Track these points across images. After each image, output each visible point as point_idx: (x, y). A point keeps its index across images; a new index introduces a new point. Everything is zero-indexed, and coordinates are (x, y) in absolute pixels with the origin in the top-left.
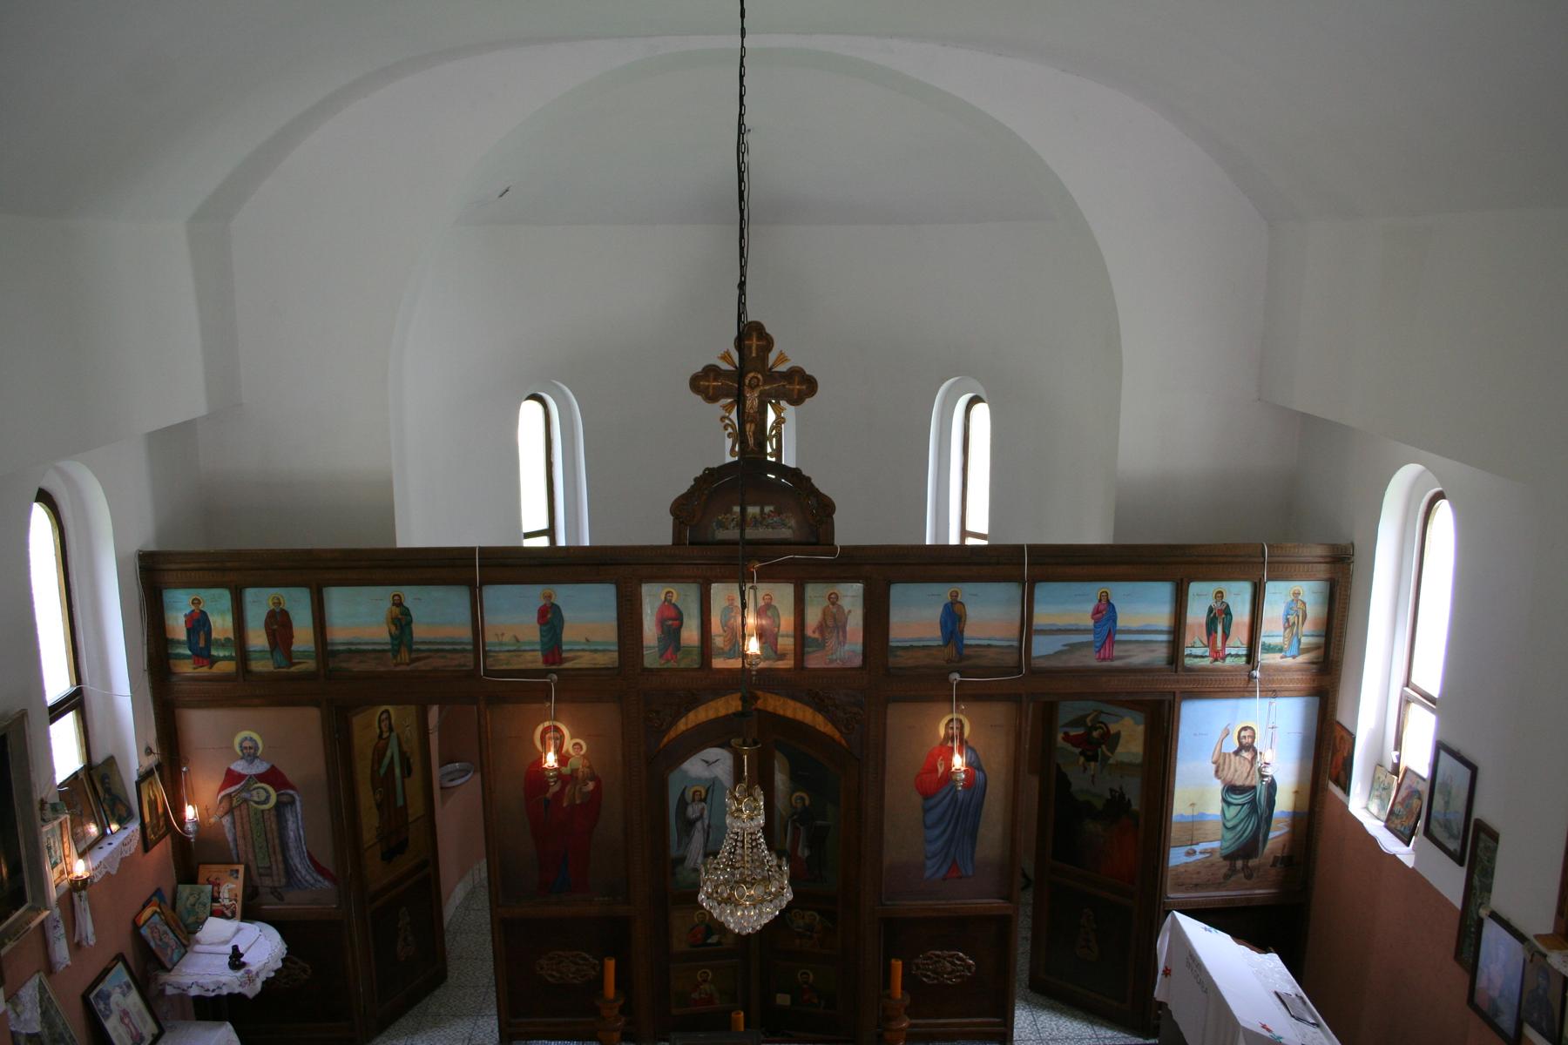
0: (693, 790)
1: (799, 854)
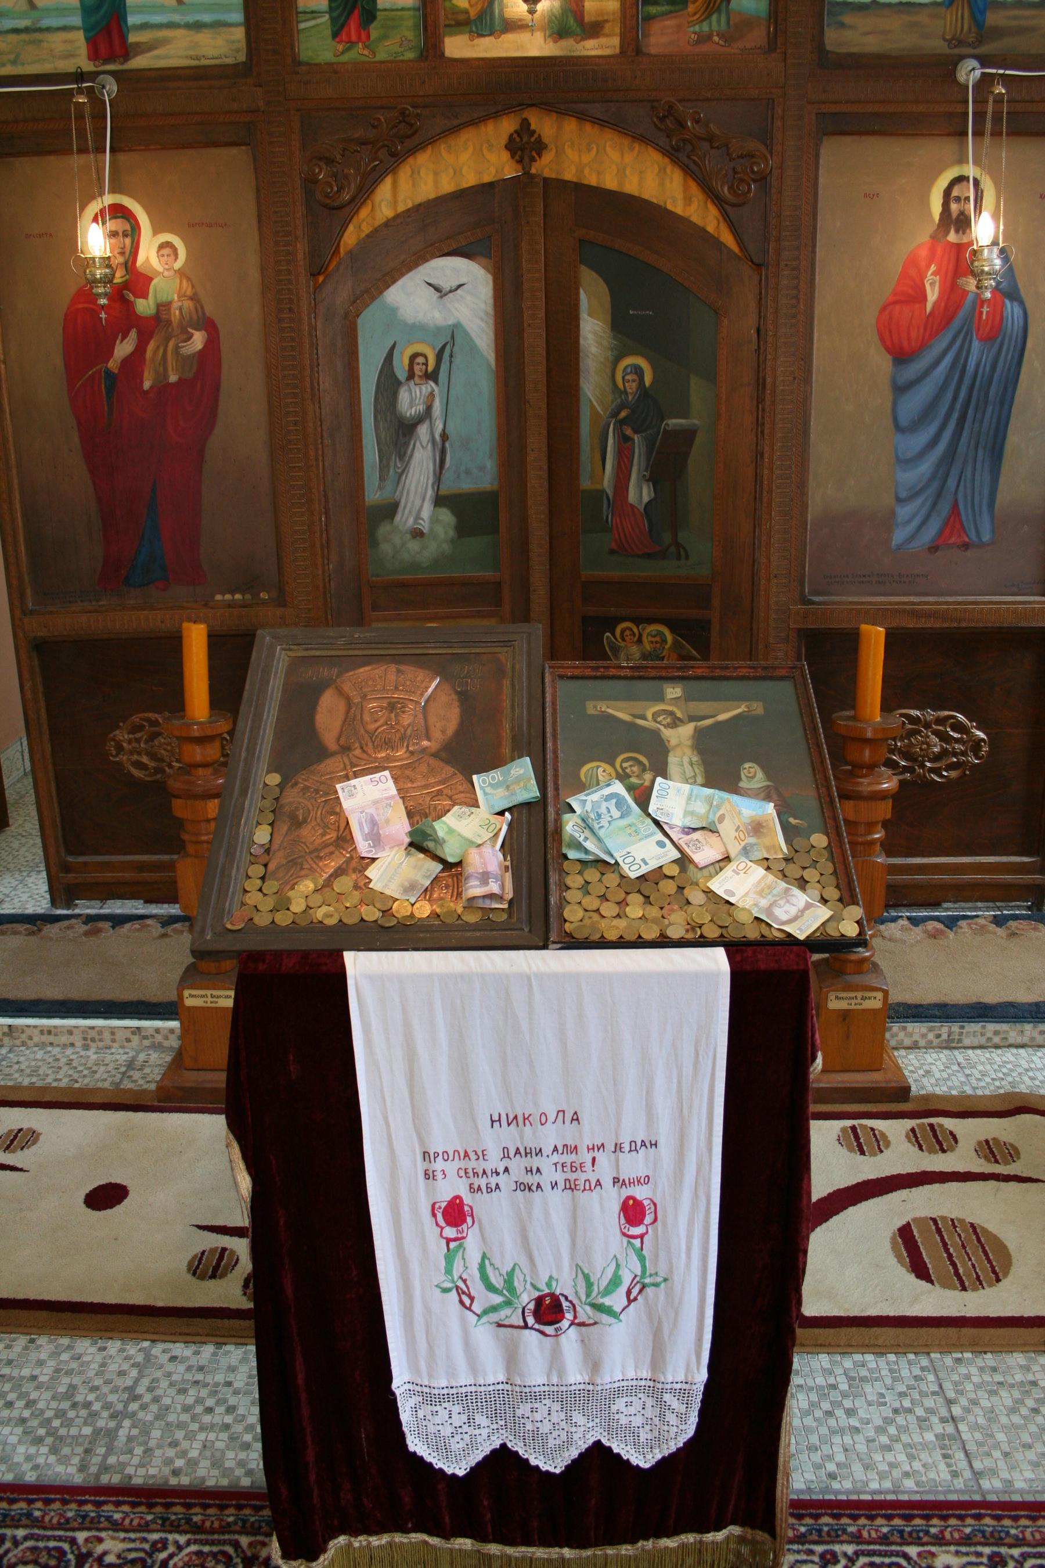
0: (409, 352)
1: (632, 497)
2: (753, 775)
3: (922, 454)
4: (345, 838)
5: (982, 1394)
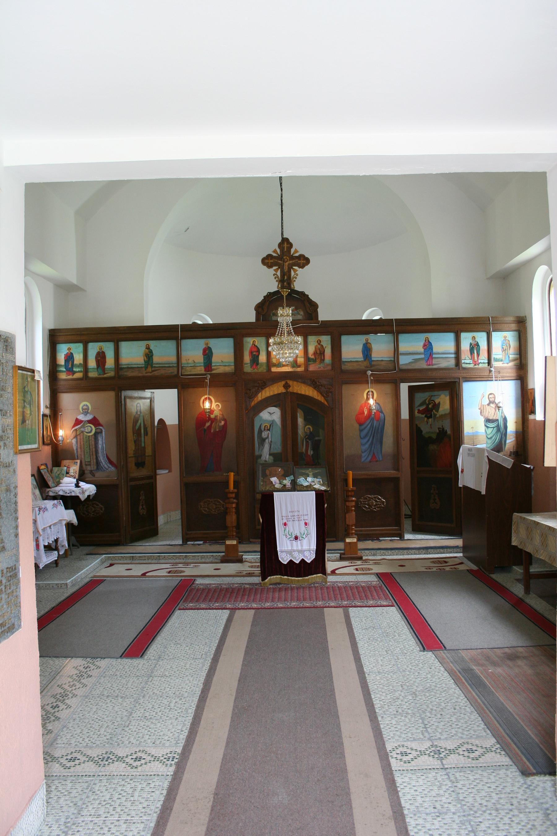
0: (264, 425)
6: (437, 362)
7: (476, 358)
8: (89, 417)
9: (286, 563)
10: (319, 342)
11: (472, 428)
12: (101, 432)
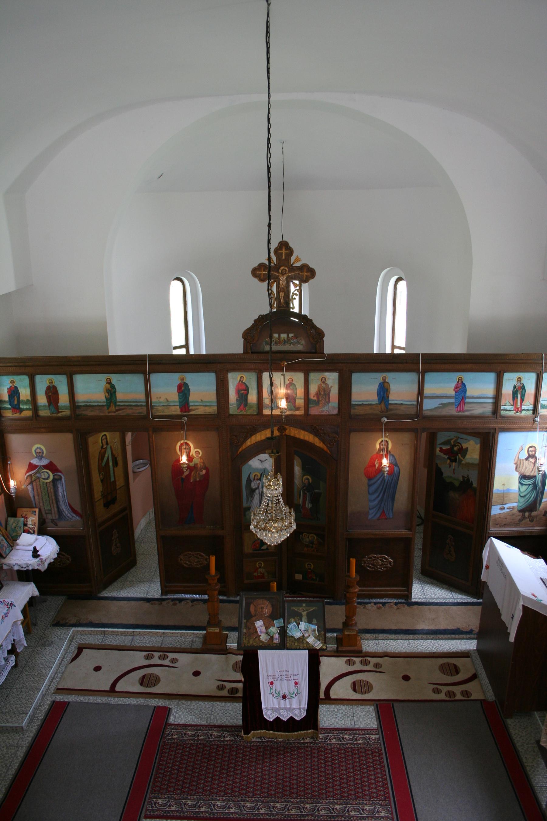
1: (307, 506)
2: (315, 621)
3: (374, 500)
4: (256, 632)
5: (360, 713)
6: (471, 407)
7: (519, 404)
8: (45, 462)
9: (271, 720)
10: (324, 380)
11: (504, 485)
12: (60, 479)
